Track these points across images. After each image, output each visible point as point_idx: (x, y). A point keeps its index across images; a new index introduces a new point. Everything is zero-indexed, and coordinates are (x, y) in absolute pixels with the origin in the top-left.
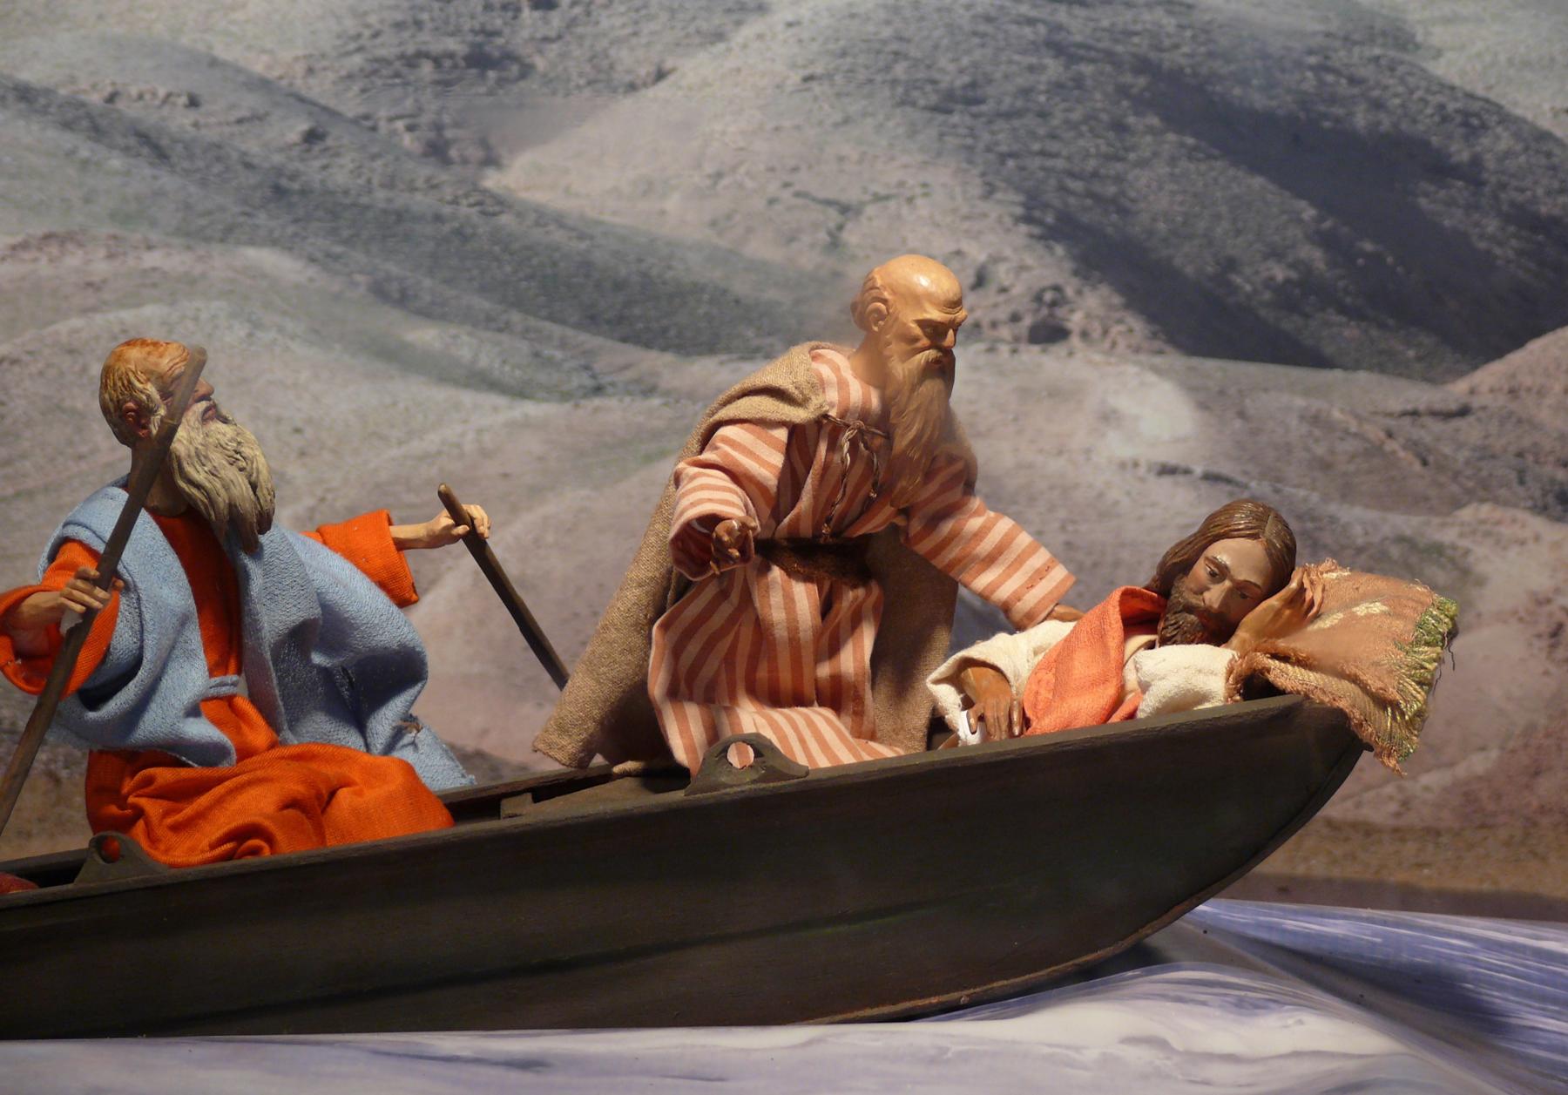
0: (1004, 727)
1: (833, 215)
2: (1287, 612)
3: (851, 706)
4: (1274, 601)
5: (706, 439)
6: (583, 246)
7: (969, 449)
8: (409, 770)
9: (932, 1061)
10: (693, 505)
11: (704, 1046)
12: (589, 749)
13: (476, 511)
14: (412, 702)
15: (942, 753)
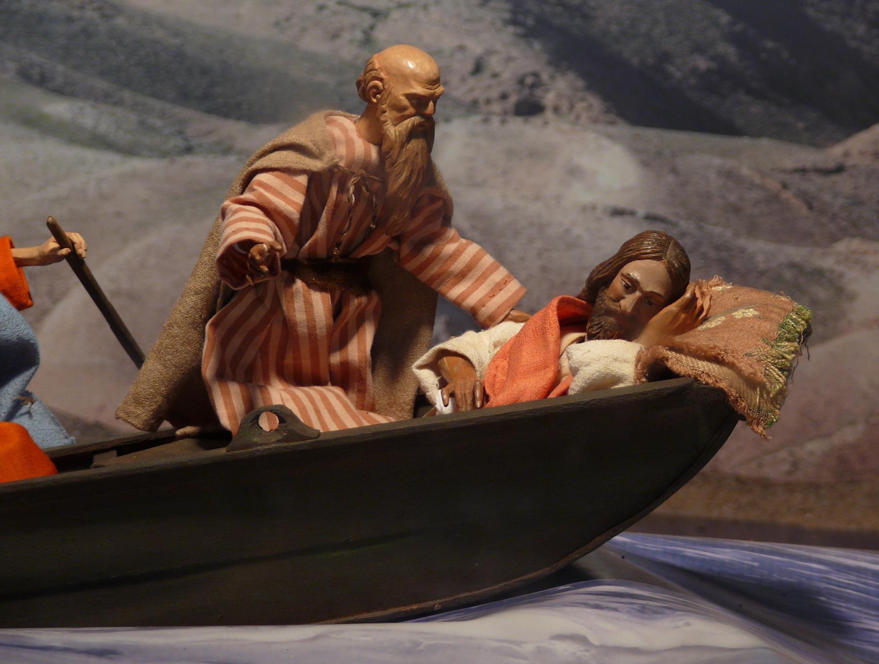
0: (469, 401)
1: (366, 20)
2: (683, 316)
3: (356, 385)
4: (673, 307)
5: (246, 183)
6: (177, 41)
7: (446, 192)
8: (24, 432)
9: (409, 652)
10: (234, 232)
11: (236, 640)
12: (158, 417)
13: (76, 238)
14: (28, 382)
15: (425, 420)
